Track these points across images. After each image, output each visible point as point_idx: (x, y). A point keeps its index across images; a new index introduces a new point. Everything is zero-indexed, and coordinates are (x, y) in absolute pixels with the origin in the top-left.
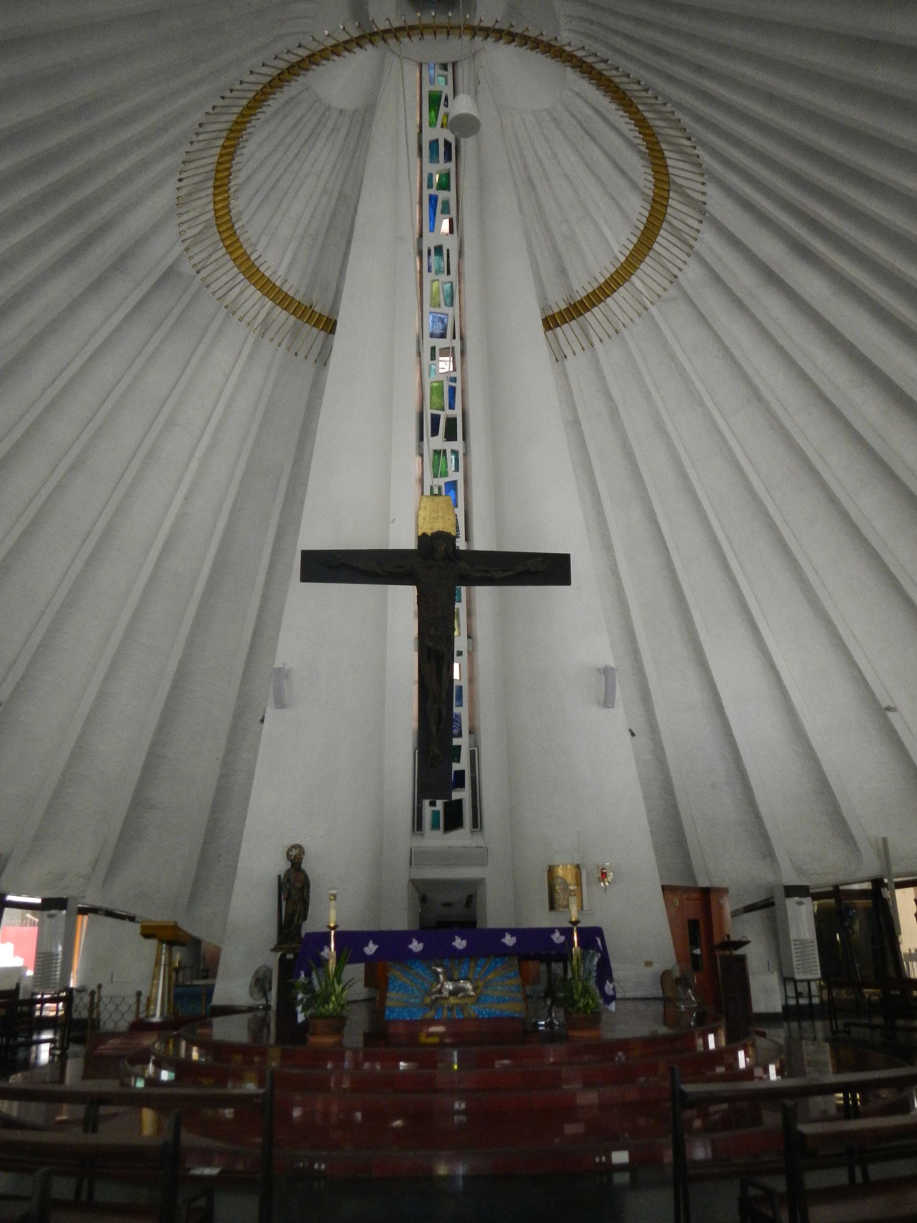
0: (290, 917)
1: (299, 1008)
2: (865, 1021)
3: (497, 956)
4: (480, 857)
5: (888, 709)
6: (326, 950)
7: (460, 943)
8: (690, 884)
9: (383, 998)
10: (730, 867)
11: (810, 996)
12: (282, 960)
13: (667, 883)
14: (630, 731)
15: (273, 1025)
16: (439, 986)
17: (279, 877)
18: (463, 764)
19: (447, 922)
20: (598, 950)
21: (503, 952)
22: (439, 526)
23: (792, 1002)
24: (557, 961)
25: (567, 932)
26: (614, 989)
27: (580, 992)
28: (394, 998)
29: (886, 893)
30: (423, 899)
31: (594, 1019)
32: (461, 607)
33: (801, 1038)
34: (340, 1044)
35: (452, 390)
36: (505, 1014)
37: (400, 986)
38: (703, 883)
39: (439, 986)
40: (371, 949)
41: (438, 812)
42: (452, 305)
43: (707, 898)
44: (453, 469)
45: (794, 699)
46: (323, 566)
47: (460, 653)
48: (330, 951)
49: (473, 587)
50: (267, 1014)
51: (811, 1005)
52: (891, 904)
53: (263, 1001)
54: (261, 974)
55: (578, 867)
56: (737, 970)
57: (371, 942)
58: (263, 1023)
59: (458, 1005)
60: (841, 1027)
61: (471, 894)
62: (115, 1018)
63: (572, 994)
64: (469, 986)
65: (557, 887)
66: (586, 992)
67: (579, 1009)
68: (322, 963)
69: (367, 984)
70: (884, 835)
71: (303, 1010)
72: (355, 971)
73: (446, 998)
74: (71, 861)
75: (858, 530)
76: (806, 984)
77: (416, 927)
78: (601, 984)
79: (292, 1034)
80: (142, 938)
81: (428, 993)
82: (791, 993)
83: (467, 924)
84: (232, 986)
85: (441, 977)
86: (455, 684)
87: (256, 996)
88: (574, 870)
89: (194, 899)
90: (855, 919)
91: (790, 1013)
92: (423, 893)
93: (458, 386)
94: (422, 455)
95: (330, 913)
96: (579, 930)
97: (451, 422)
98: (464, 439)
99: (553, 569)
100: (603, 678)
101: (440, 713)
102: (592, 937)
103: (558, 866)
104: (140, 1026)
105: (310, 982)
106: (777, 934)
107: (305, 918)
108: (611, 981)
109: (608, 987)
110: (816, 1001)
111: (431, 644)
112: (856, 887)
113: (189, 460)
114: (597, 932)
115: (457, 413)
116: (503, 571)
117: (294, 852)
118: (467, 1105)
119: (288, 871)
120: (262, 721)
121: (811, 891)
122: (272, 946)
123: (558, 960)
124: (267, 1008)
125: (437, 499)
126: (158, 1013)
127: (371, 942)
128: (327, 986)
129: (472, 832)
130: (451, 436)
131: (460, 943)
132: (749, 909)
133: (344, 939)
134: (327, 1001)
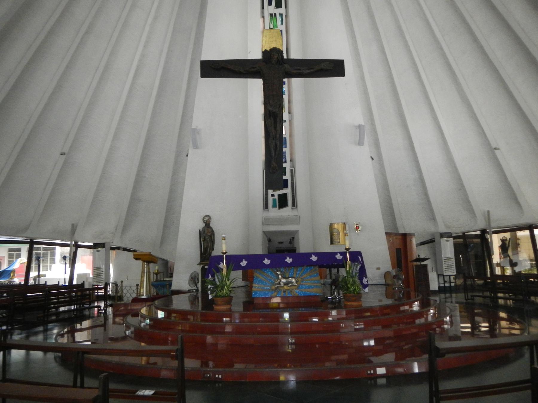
0: (206, 249)
1: (209, 292)
2: (481, 294)
3: (307, 266)
4: (296, 220)
5: (495, 149)
6: (222, 264)
7: (289, 260)
8: (395, 232)
9: (251, 287)
10: (415, 224)
11: (450, 283)
12: (203, 269)
13: (388, 232)
14: (371, 157)
15: (200, 299)
16: (279, 281)
17: (200, 230)
18: (287, 176)
19: (282, 252)
20: (360, 263)
21: (312, 264)
22: (273, 45)
23: (442, 285)
24: (334, 268)
25: (343, 254)
26: (367, 282)
28: (256, 286)
29: (488, 236)
30: (270, 240)
31: (358, 296)
32: (285, 88)
33: (446, 302)
34: (230, 310)
36: (312, 294)
38: (401, 231)
39: (279, 281)
40: (244, 263)
42: (281, 7)
43: (405, 238)
44: (280, 23)
45: (449, 144)
46: (213, 69)
47: (285, 121)
48: (223, 265)
50: (197, 293)
51: (450, 286)
52: (489, 240)
53: (195, 288)
55: (344, 223)
56: (423, 272)
58: (196, 297)
59: (288, 290)
60: (470, 297)
61: (292, 237)
62: (128, 296)
63: (347, 284)
64: (294, 280)
66: (354, 283)
67: (351, 291)
68: (219, 270)
69: (243, 280)
70: (487, 209)
71: (211, 294)
72: (239, 274)
73: (282, 287)
74: (106, 227)
75: (488, 57)
76: (448, 277)
77: (266, 253)
78: (361, 279)
79: (208, 304)
80: (135, 260)
81: (274, 284)
82: (442, 281)
83: (292, 251)
84: (181, 281)
85: (280, 276)
86: (284, 136)
87: (191, 286)
88: (343, 225)
89: (163, 241)
90: (472, 249)
91: (442, 290)
92: (269, 237)
94: (263, 17)
95: (223, 247)
96: (350, 253)
98: (286, 7)
99: (335, 68)
100: (358, 130)
101: (276, 145)
102: (356, 256)
104: (137, 300)
105: (214, 280)
106: (436, 255)
107: (213, 249)
108: (366, 278)
109: (365, 281)
110: (453, 285)
111: (270, 109)
112: (474, 233)
113: (145, 26)
114: (359, 254)
116: (308, 69)
117: (206, 219)
118: (295, 340)
119: (204, 228)
120: (187, 155)
121: (453, 235)
122: (198, 263)
123: (338, 267)
124: (197, 290)
125: (272, 30)
126: (145, 294)
128: (222, 281)
131: (289, 260)
132: (422, 244)
133: (230, 259)
134: (223, 288)
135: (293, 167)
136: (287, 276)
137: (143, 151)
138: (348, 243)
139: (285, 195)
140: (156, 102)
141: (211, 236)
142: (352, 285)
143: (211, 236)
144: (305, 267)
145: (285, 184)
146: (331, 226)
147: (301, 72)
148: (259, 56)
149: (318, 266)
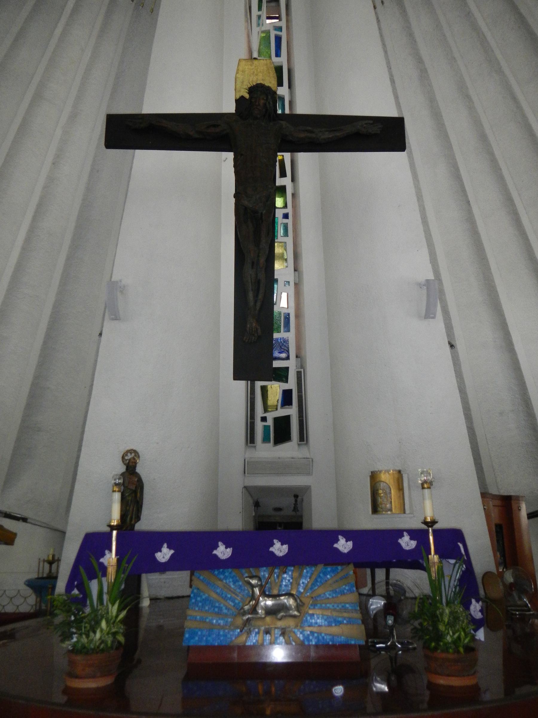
7: (279, 549)
14: (450, 343)
27: (446, 620)
30: (257, 504)
35: (278, 39)
37: (204, 601)
38: (504, 492)
41: (269, 426)
49: (296, 154)
55: (399, 472)
57: (165, 545)
61: (298, 496)
64: (291, 602)
65: (380, 492)
92: (256, 497)
93: (283, 34)
96: (434, 531)
98: (290, 86)
100: (424, 291)
101: (258, 282)
103: (380, 472)
111: (246, 203)
115: (283, 60)
117: (129, 456)
120: (100, 334)
125: (256, 62)
127: (165, 545)
129: (299, 445)
135: (302, 367)
136: (275, 592)
137: (45, 343)
138: (426, 508)
139: (287, 419)
140: (69, 258)
141: (135, 492)
142: (450, 625)
143: (135, 492)
144: (320, 567)
145: (281, 375)
146: (374, 477)
147: (313, 135)
148: (230, 108)
149: (351, 566)
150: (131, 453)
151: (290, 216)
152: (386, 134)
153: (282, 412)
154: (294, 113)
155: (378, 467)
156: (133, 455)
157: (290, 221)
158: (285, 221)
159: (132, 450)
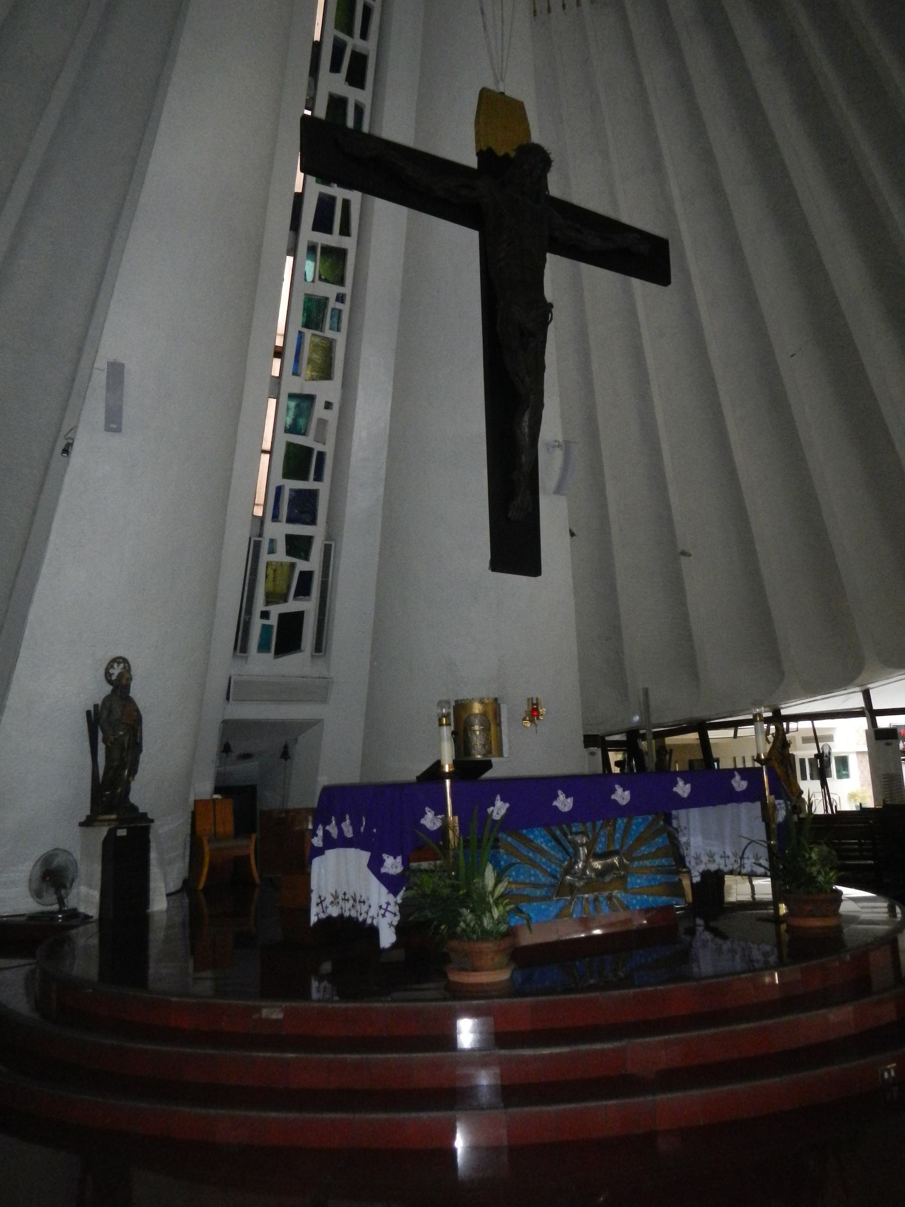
5: (684, 553)
41: (271, 627)
54: (57, 862)
57: (498, 797)
97: (359, 60)
103: (471, 701)
117: (116, 671)
120: (66, 451)
127: (498, 797)
130: (356, 78)
150: (119, 663)
151: (348, 299)
152: (642, 256)
153: (292, 606)
154: (376, 133)
155: (464, 694)
156: (122, 665)
157: (345, 308)
158: (339, 306)
159: (120, 658)
